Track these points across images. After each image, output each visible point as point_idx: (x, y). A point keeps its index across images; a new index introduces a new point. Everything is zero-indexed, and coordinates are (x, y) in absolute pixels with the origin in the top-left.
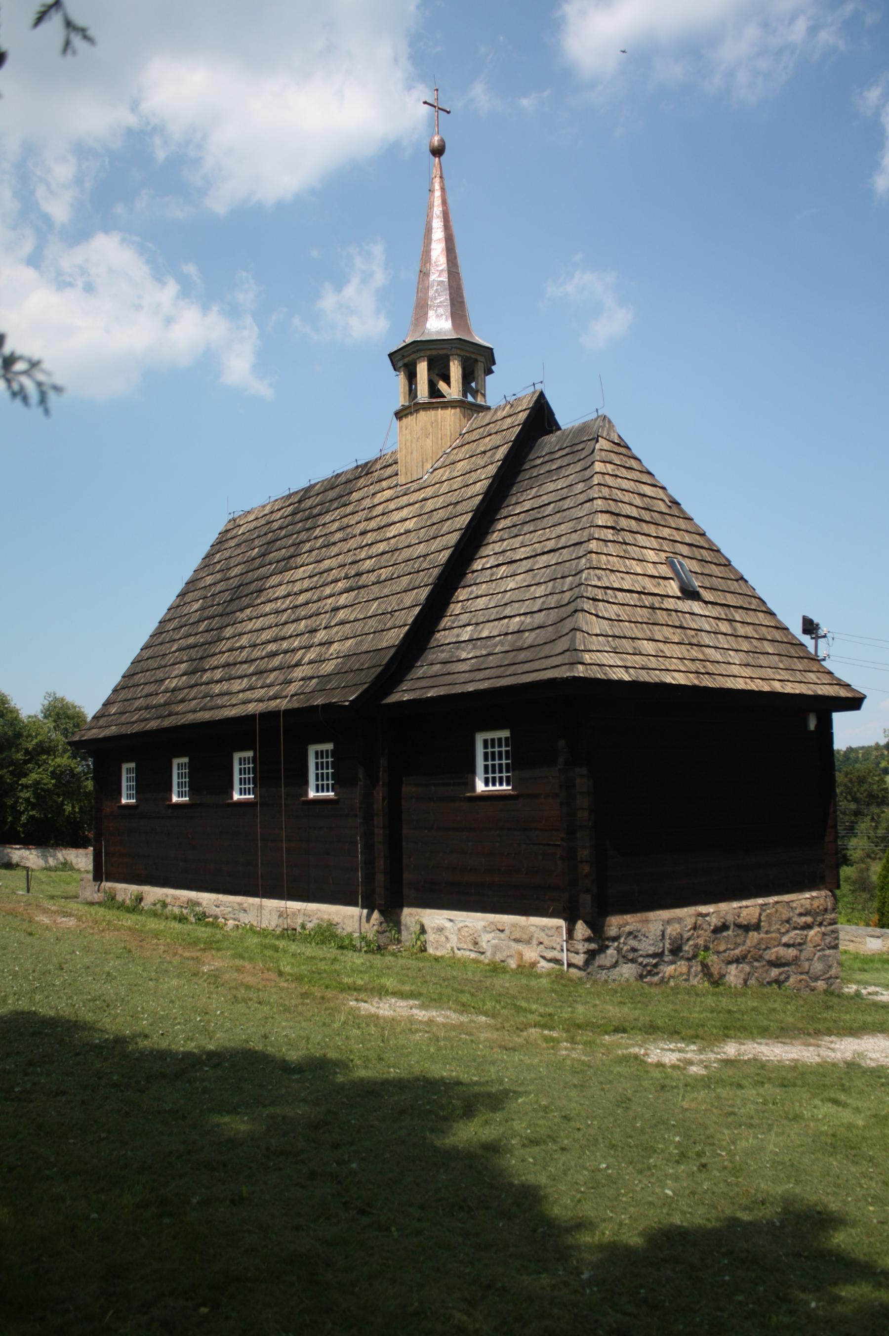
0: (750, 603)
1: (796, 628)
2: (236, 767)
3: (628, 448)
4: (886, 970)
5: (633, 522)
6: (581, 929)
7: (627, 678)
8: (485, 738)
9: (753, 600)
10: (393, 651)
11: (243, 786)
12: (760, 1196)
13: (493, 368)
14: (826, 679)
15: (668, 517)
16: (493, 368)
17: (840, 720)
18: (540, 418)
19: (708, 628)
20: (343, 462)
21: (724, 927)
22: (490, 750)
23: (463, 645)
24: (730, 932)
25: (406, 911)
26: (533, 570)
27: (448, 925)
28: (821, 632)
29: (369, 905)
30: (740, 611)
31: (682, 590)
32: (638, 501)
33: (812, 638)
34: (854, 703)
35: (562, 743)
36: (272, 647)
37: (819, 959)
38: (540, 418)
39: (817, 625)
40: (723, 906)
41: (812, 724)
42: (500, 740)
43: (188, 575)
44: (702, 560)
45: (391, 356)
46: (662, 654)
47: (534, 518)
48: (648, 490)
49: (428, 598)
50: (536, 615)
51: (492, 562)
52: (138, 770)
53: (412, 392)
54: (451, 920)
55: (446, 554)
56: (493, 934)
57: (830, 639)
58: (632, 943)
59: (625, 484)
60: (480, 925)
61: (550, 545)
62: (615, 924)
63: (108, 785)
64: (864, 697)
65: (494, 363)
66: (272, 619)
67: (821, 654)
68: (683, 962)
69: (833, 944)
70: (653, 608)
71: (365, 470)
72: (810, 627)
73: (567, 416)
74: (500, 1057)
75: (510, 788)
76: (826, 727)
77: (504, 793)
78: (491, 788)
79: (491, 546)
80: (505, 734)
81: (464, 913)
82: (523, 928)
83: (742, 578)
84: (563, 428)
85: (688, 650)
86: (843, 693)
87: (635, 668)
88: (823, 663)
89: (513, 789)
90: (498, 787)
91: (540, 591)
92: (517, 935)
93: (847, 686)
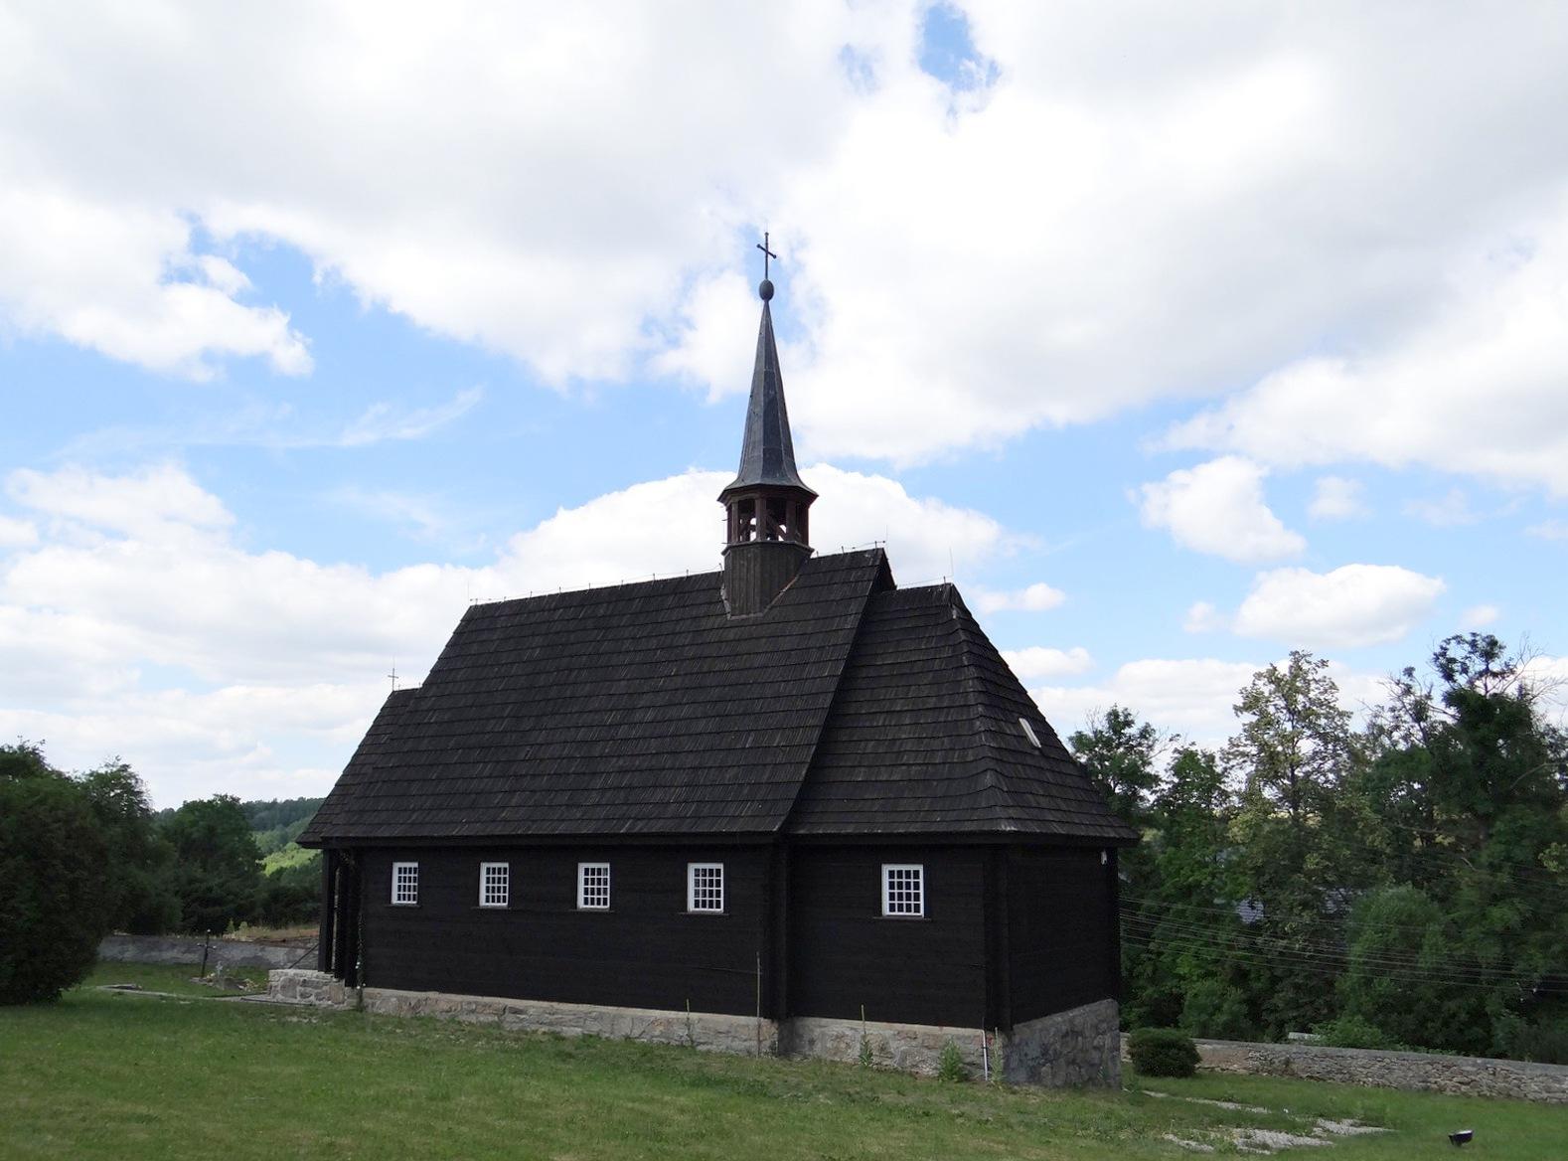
56: (903, 1042)
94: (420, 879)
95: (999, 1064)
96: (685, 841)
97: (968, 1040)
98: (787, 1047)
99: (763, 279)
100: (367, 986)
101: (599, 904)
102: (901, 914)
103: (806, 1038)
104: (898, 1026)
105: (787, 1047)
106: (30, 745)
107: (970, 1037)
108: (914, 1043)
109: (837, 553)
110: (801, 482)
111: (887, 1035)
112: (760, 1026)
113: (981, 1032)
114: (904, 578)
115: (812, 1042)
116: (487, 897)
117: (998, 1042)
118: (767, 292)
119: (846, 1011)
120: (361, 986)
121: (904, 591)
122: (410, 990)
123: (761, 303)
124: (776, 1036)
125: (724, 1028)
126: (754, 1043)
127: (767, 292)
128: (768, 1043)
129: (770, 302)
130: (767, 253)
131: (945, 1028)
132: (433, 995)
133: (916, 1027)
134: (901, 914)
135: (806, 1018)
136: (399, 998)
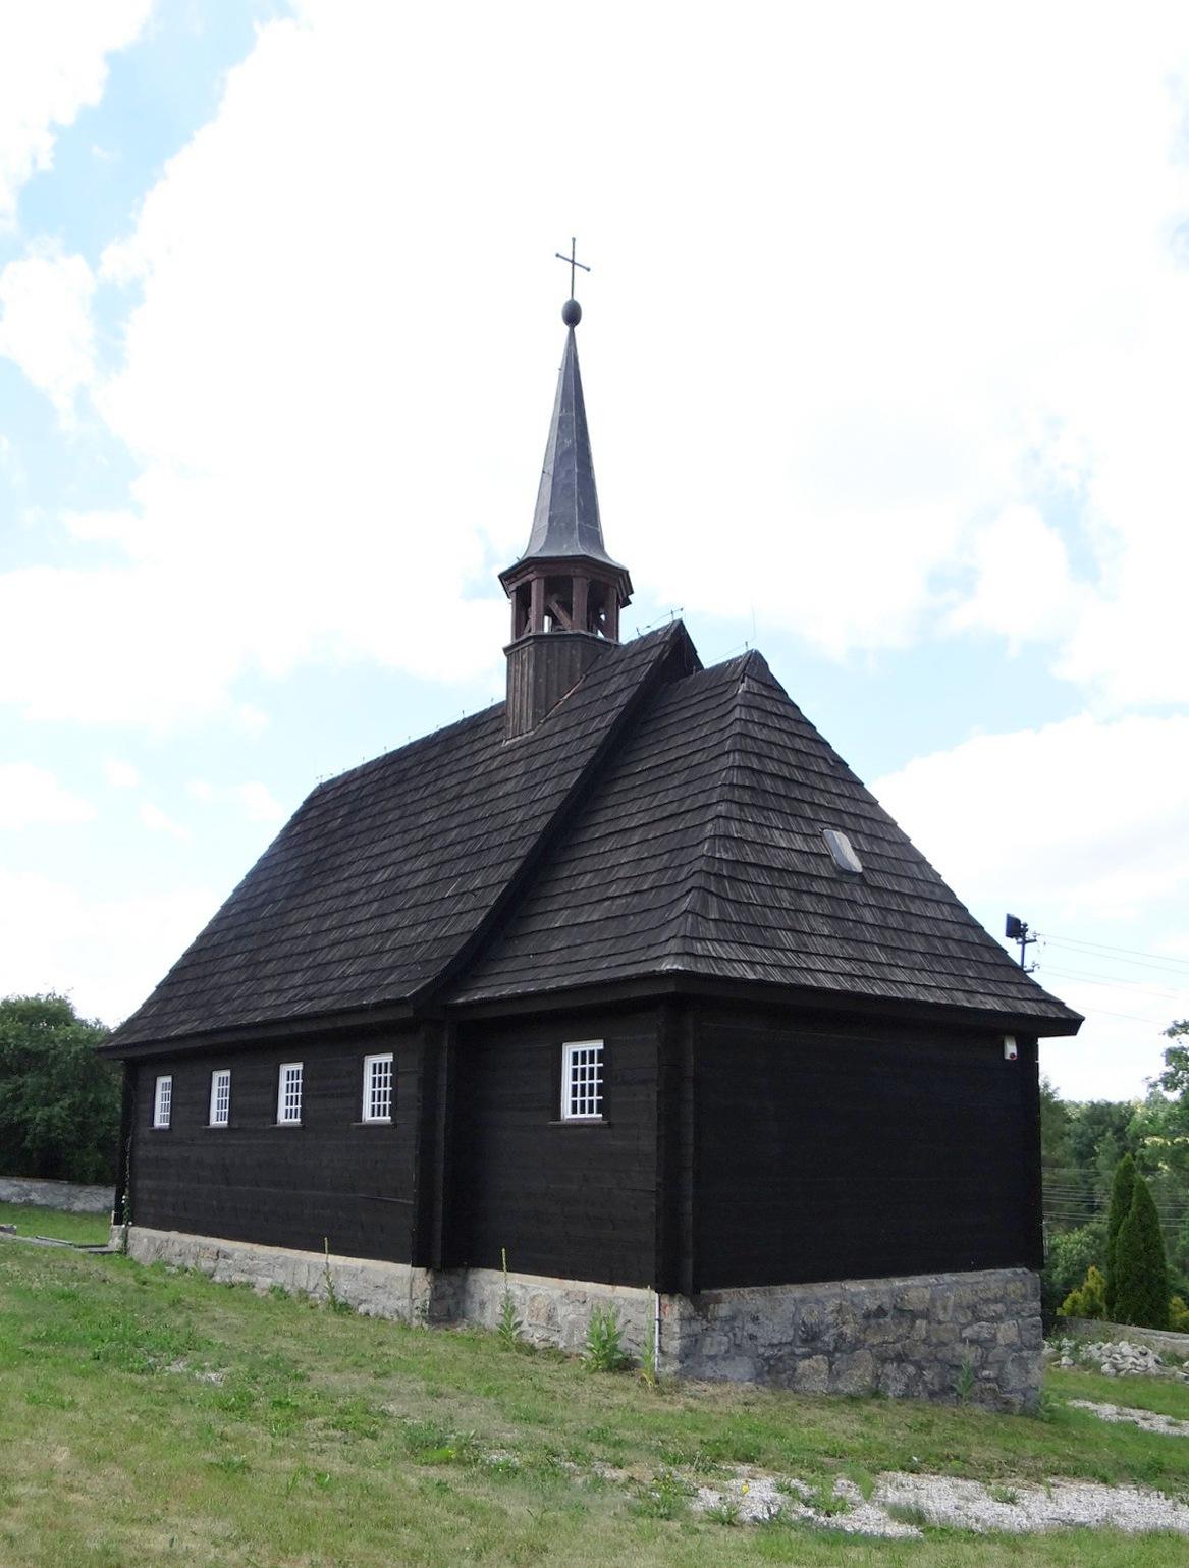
0: (933, 893)
1: (996, 931)
2: (283, 1083)
4: (3, 1470)
5: (780, 783)
7: (751, 976)
8: (575, 1050)
9: (937, 890)
10: (465, 940)
11: (289, 1107)
13: (630, 597)
15: (828, 780)
16: (630, 597)
17: (1049, 1049)
19: (871, 920)
21: (881, 1312)
22: (579, 1066)
23: (556, 932)
24: (888, 1320)
26: (648, 840)
28: (1029, 936)
30: (917, 901)
33: (1018, 943)
34: (1067, 1023)
36: (335, 935)
37: (1013, 1361)
39: (1025, 925)
40: (881, 1284)
41: (1011, 1049)
42: (592, 1053)
44: (871, 836)
45: (506, 577)
46: (804, 949)
48: (799, 744)
49: (517, 873)
50: (645, 895)
52: (174, 1087)
54: (522, 1287)
55: (546, 820)
56: (571, 1308)
57: (1042, 944)
58: (750, 1328)
59: (776, 737)
60: (557, 1294)
61: (672, 809)
62: (732, 1301)
63: (137, 1099)
64: (1083, 1019)
65: (632, 592)
66: (341, 903)
67: (1028, 966)
68: (820, 1357)
69: (1034, 1342)
70: (799, 892)
72: (1015, 929)
75: (601, 1115)
76: (1029, 1055)
77: (595, 1121)
78: (579, 1115)
79: (603, 813)
80: (597, 1046)
81: (539, 1278)
82: (610, 1304)
84: (705, 667)
85: (842, 947)
86: (1052, 1013)
87: (764, 964)
88: (1029, 975)
89: (603, 1119)
90: (587, 1115)
94: (394, 1096)
95: (674, 1346)
96: (299, 1029)
97: (637, 1308)
98: (446, 1310)
99: (569, 297)
100: (133, 1225)
101: (583, 1111)
102: (582, 1116)
103: (476, 1299)
104: (569, 1284)
105: (446, 1310)
106: (60, 994)
107: (643, 1303)
108: (583, 1310)
109: (633, 638)
110: (609, 559)
111: (555, 1297)
112: (413, 1279)
113: (648, 1295)
114: (710, 655)
115: (482, 1304)
116: (574, 1104)
117: (675, 1309)
118: (572, 315)
119: (523, 1264)
120: (127, 1225)
121: (711, 669)
122: (160, 1229)
123: (566, 329)
124: (428, 1292)
125: (381, 1281)
126: (406, 1302)
127: (572, 315)
128: (418, 1303)
129: (576, 329)
130: (573, 262)
131: (618, 1287)
132: (174, 1235)
133: (589, 1287)
134: (582, 1116)
135: (475, 1271)
136: (152, 1240)
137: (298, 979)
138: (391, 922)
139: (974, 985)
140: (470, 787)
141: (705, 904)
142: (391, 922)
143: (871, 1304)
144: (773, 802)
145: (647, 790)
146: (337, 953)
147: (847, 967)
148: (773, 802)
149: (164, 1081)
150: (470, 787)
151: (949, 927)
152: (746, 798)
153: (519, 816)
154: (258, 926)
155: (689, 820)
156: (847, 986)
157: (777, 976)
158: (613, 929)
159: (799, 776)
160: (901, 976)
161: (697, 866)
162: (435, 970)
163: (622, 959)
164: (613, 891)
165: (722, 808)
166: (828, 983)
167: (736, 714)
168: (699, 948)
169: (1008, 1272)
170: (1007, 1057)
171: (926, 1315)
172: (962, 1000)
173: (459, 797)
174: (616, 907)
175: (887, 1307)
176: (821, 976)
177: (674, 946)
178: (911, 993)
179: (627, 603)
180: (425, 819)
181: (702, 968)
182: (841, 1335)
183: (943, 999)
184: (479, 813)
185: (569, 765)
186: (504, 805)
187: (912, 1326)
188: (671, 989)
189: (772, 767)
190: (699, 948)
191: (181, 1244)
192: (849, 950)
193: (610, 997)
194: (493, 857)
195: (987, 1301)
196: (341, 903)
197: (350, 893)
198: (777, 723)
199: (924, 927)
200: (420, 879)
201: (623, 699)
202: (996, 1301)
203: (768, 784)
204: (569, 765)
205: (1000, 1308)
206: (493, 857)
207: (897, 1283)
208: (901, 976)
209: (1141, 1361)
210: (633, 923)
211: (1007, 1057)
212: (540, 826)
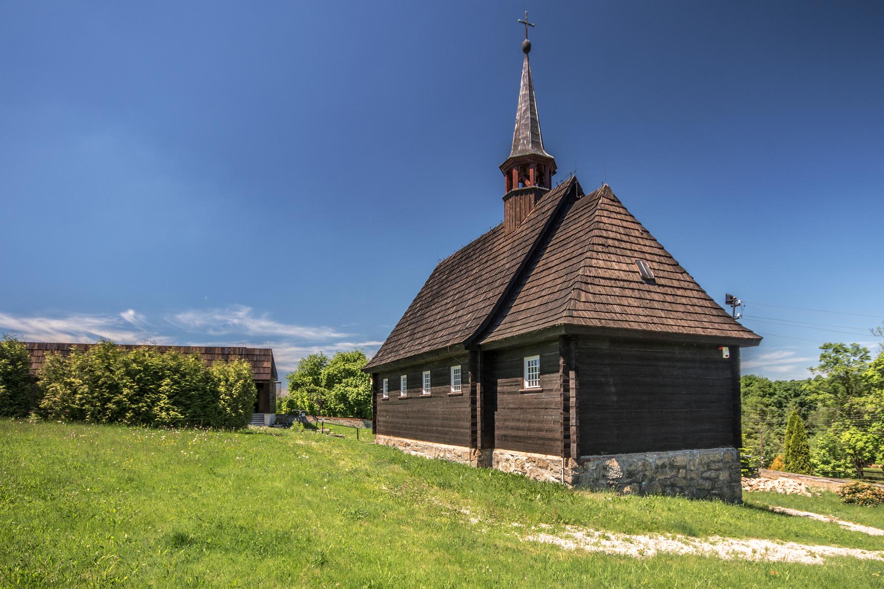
1: (721, 303)
3: (619, 202)
6: (572, 463)
7: (599, 324)
12: (280, 534)
14: (736, 328)
18: (574, 192)
20: (485, 230)
21: (663, 466)
25: (497, 451)
27: (511, 458)
29: (473, 445)
31: (643, 278)
32: (621, 230)
34: (755, 341)
35: (561, 361)
38: (574, 192)
41: (726, 353)
43: (419, 291)
47: (564, 244)
51: (541, 269)
53: (510, 186)
60: (525, 458)
61: (568, 257)
66: (444, 308)
71: (494, 232)
72: (731, 300)
73: (588, 191)
74: (377, 488)
82: (544, 461)
83: (685, 272)
86: (746, 336)
91: (559, 281)
92: (541, 464)
93: (750, 332)
104: (529, 454)
105: (486, 462)
132: (391, 437)
137: (427, 338)
138: (460, 313)
139: (707, 325)
140: (491, 257)
141: (579, 295)
142: (460, 313)
143: (660, 463)
144: (612, 250)
145: (561, 249)
146: (440, 327)
147: (645, 319)
148: (612, 250)
149: (386, 380)
150: (491, 257)
151: (696, 300)
152: (600, 250)
153: (507, 266)
154: (416, 319)
155: (575, 261)
156: (644, 327)
157: (612, 324)
158: (542, 309)
159: (625, 238)
160: (671, 322)
161: (578, 279)
162: (473, 331)
163: (544, 321)
164: (543, 293)
165: (588, 254)
166: (635, 326)
167: (597, 213)
168: (575, 313)
169: (725, 449)
170: (724, 357)
171: (685, 467)
172: (700, 332)
173: (486, 262)
174: (545, 300)
175: (667, 464)
176: (632, 324)
177: (564, 314)
178: (675, 329)
179: (554, 173)
180: (474, 271)
181: (575, 322)
182: (644, 475)
183: (692, 331)
184: (493, 267)
185: (527, 243)
186: (502, 262)
187: (678, 472)
188: (563, 332)
189: (612, 235)
190: (575, 313)
191: (394, 440)
192: (647, 312)
193: (543, 338)
194: (497, 284)
195: (714, 462)
196: (444, 308)
197: (447, 304)
198: (614, 215)
199: (684, 300)
200: (471, 295)
201: (550, 213)
202: (719, 462)
203: (610, 242)
204: (527, 243)
205: (721, 465)
206: (497, 284)
207: (671, 453)
208: (671, 322)
209: (799, 487)
210: (550, 306)
211: (724, 357)
212: (515, 269)
